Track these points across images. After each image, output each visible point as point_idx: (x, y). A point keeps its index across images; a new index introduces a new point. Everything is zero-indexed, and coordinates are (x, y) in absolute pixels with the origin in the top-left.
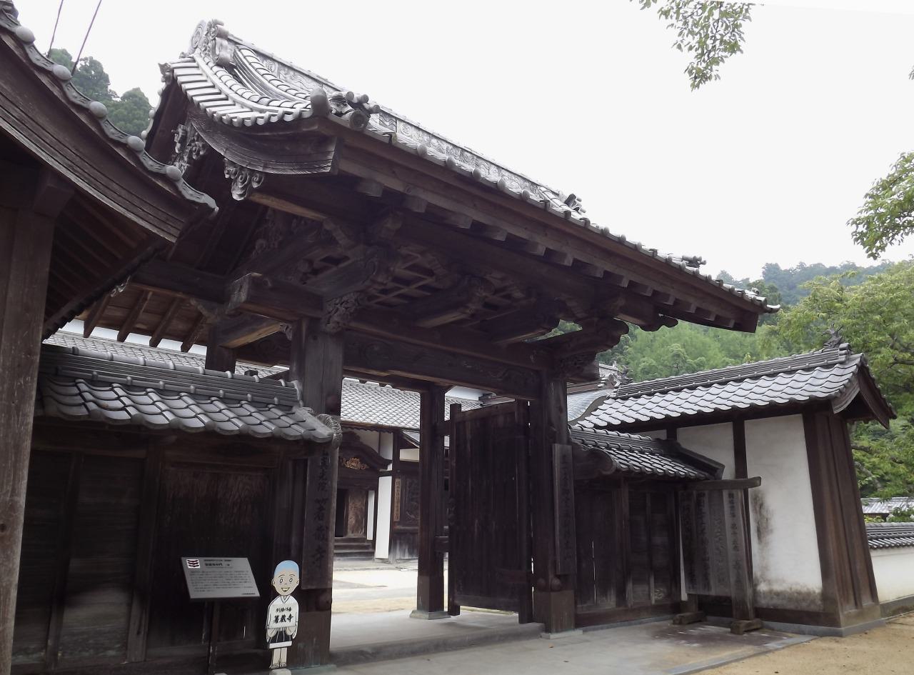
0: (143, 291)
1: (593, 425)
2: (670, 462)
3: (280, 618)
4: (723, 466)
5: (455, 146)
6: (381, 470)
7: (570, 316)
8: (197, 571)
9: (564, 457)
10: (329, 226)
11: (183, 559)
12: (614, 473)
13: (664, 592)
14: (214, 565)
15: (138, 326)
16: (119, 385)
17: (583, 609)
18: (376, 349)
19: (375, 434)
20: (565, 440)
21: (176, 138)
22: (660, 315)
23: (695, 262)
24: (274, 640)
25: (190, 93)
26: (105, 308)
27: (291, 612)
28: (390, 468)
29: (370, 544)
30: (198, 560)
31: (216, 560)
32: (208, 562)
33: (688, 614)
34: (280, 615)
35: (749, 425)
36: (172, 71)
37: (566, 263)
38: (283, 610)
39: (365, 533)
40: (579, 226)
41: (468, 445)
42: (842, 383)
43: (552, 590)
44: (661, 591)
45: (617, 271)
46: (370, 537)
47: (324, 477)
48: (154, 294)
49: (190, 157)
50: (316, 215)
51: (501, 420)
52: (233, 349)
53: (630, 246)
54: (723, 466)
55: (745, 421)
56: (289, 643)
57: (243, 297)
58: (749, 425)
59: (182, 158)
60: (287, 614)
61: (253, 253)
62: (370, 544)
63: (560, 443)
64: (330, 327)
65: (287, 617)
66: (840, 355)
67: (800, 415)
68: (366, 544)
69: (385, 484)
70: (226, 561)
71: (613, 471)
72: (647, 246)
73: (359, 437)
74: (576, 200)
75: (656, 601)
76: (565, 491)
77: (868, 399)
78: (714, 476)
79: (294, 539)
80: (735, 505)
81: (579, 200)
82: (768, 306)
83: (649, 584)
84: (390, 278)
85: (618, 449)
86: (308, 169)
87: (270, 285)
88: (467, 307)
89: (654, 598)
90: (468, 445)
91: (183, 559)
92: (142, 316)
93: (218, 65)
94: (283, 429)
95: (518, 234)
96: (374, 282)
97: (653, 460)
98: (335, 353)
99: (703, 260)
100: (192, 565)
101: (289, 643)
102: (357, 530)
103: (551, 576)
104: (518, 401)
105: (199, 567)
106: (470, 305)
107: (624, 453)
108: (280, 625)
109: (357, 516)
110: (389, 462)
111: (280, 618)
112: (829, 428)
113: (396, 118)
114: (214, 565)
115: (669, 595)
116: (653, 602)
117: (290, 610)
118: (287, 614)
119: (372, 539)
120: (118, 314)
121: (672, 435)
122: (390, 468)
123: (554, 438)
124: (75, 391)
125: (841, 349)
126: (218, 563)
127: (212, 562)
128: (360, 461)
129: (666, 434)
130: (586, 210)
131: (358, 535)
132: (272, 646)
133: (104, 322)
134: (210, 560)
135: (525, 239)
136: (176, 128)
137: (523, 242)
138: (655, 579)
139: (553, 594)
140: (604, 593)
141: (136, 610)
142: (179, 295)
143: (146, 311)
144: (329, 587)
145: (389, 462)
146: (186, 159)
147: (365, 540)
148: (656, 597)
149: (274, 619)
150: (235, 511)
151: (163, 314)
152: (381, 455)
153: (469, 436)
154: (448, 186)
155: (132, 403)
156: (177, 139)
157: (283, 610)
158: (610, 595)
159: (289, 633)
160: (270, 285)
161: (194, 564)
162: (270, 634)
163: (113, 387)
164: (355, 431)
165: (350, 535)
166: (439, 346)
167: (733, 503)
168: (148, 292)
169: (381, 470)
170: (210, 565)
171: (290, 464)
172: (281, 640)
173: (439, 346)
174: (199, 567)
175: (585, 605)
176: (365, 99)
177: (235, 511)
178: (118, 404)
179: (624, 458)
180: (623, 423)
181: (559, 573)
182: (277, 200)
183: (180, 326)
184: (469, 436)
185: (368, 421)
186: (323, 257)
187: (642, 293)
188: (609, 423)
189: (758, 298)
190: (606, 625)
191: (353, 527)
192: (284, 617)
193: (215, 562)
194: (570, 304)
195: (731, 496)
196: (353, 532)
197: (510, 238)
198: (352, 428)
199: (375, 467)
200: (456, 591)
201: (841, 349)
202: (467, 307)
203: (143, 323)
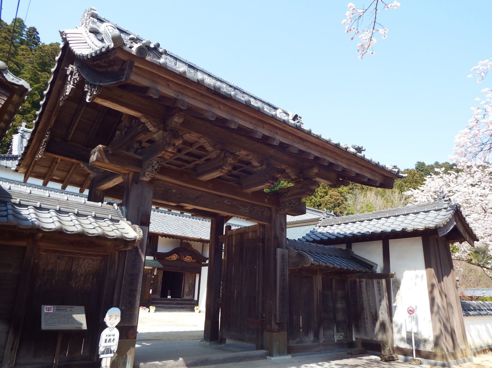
0: (55, 158)
1: (305, 240)
2: (346, 262)
3: (108, 340)
4: (377, 265)
5: (231, 86)
6: (203, 263)
7: (288, 178)
8: (50, 313)
9: (283, 256)
10: (143, 120)
11: (42, 306)
12: (310, 266)
13: (342, 335)
14: (62, 310)
15: (54, 178)
16: (109, 220)
17: (293, 343)
18: (174, 191)
19: (200, 244)
20: (285, 247)
21: (68, 72)
22: (341, 179)
23: (359, 150)
24: (103, 353)
25: (72, 48)
26: (34, 166)
27: (115, 337)
28: (207, 262)
29: (196, 302)
30: (52, 307)
31: (64, 307)
32: (58, 308)
33: (358, 349)
34: (108, 338)
35: (392, 242)
36: (66, 34)
37: (275, 143)
38: (109, 336)
39: (194, 296)
40: (394, 174)
41: (234, 249)
42: (444, 220)
43: (274, 332)
44: (340, 335)
45: (308, 150)
46: (196, 299)
47: (136, 261)
48: (61, 160)
49: (74, 82)
50: (137, 114)
51: (250, 235)
52: (103, 191)
53: (334, 145)
54: (377, 265)
55: (389, 240)
56: (112, 355)
57: (95, 159)
58: (392, 242)
59: (70, 83)
60: (112, 338)
61: (114, 139)
62: (196, 302)
63: (282, 247)
64: (146, 179)
65: (112, 339)
66: (445, 204)
67: (421, 237)
68: (193, 302)
69: (205, 271)
70: (70, 307)
71: (310, 264)
72: (334, 141)
73: (191, 245)
74: (298, 118)
75: (337, 341)
76: (283, 275)
77: (461, 229)
78: (371, 270)
79: (115, 297)
80: (380, 288)
81: (300, 118)
82: (400, 174)
83: (333, 331)
84: (176, 150)
85: (323, 254)
86: (116, 80)
87: (110, 152)
88: (223, 169)
89: (336, 338)
90: (234, 249)
91: (42, 306)
92: (56, 172)
93: (90, 32)
94: (123, 234)
95: (245, 125)
96: (167, 151)
97: (329, 259)
98: (149, 193)
99: (363, 149)
100: (47, 310)
101: (112, 355)
102: (189, 294)
103: (273, 323)
104: (259, 224)
105: (52, 311)
106: (224, 167)
107: (319, 255)
108: (108, 344)
109: (189, 287)
110: (207, 259)
111: (108, 340)
112: (438, 246)
113: (197, 69)
114: (62, 310)
115: (346, 337)
116: (336, 341)
117: (114, 335)
118: (112, 338)
119: (197, 300)
120: (43, 170)
121: (349, 247)
122: (207, 262)
123: (279, 245)
124: (5, 208)
125: (445, 201)
126: (65, 309)
127: (61, 308)
128: (192, 258)
129: (345, 246)
130: (303, 123)
131: (191, 297)
132: (101, 356)
133: (35, 175)
134: (60, 307)
135: (252, 129)
136: (68, 67)
137: (224, 121)
138: (323, 330)
139: (274, 334)
140: (306, 333)
141: (11, 336)
142: (451, 251)
143: (58, 169)
144: (134, 325)
145: (207, 259)
146: (72, 83)
147: (193, 300)
148: (338, 338)
149: (105, 340)
150: (82, 279)
151: (68, 172)
152: (203, 255)
153: (234, 243)
154: (202, 95)
155: (79, 223)
156: (68, 73)
157: (109, 336)
158: (310, 336)
159: (112, 349)
160: (110, 152)
161: (49, 309)
162: (101, 349)
163: (7, 205)
164: (189, 241)
165: (186, 297)
166: (211, 191)
167: (380, 288)
168: (58, 159)
169: (203, 263)
170: (59, 310)
171: (117, 253)
172: (107, 353)
173: (211, 191)
174: (52, 311)
175: (294, 341)
176: (362, 147)
177: (82, 279)
178: (72, 223)
179: (326, 259)
180: (322, 239)
181: (278, 322)
182: (112, 103)
183: (78, 179)
184: (234, 243)
185: (195, 237)
186: (146, 140)
187: (350, 175)
188: (314, 239)
189: (394, 170)
190: (306, 353)
191: (187, 293)
192: (110, 339)
193: (62, 308)
194: (288, 171)
195: (379, 283)
196: (187, 296)
197: (281, 144)
198: (187, 240)
199: (199, 261)
200: (224, 330)
201: (445, 201)
202: (223, 169)
203: (58, 177)
